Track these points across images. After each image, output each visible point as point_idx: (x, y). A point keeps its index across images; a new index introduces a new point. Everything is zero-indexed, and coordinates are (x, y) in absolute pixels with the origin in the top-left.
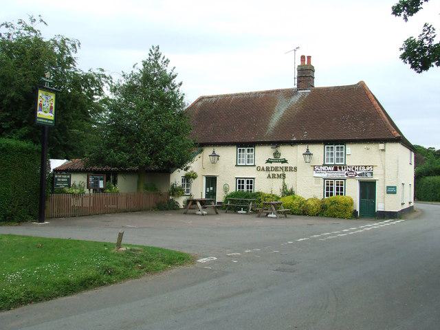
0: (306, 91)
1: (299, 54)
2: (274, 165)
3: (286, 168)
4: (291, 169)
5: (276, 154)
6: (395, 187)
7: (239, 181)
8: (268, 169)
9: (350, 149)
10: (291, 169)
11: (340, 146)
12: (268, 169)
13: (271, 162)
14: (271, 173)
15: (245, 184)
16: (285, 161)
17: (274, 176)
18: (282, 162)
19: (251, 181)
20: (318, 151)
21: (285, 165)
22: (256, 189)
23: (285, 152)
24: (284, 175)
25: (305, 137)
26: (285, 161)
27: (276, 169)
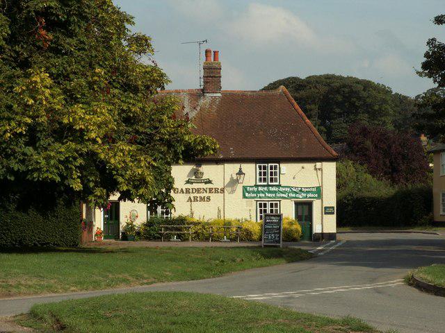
0: (215, 95)
1: (205, 47)
2: (196, 186)
3: (211, 190)
4: (216, 191)
5: (196, 173)
6: (244, 197)
7: (261, 204)
8: (188, 191)
9: (284, 167)
10: (216, 191)
11: (262, 165)
12: (188, 191)
13: (192, 183)
14: (192, 196)
15: (268, 209)
16: (210, 182)
17: (196, 199)
18: (206, 183)
19: (276, 204)
20: (250, 170)
21: (209, 186)
22: (334, 204)
23: (208, 170)
24: (209, 199)
25: (232, 154)
26: (210, 182)
27: (198, 191)
